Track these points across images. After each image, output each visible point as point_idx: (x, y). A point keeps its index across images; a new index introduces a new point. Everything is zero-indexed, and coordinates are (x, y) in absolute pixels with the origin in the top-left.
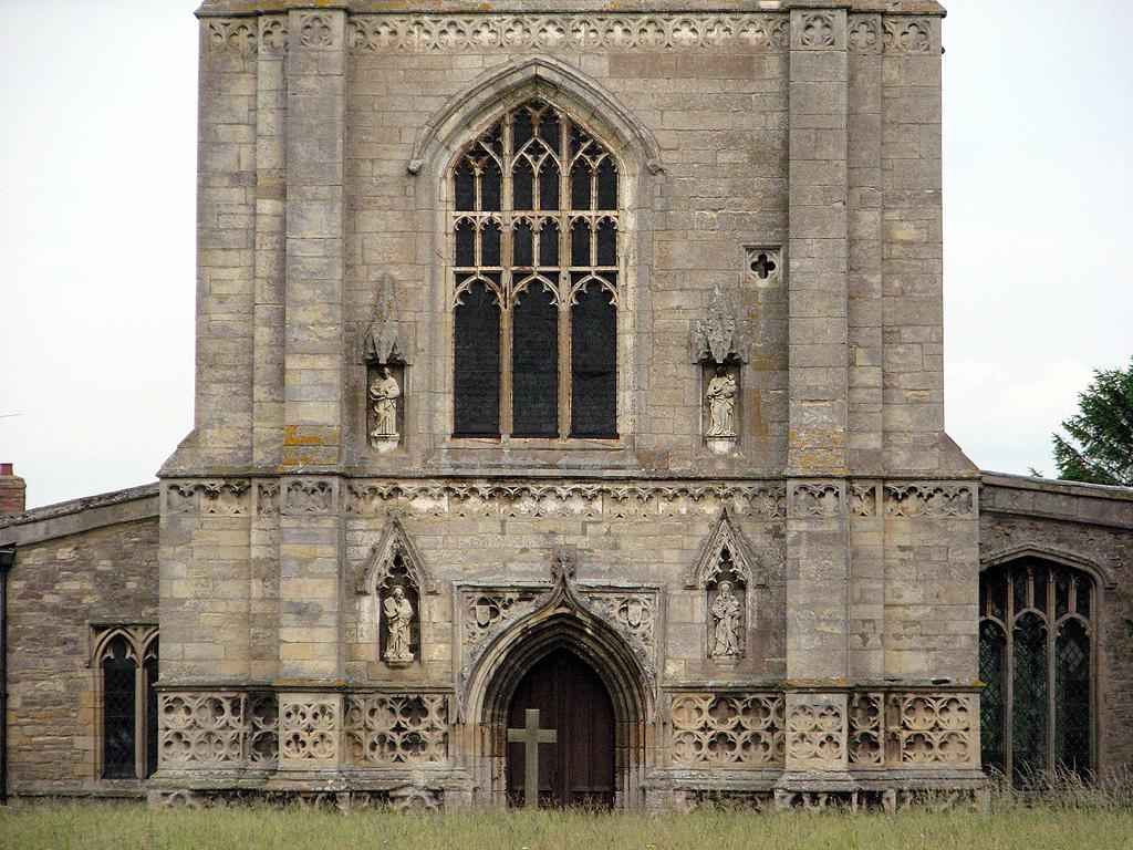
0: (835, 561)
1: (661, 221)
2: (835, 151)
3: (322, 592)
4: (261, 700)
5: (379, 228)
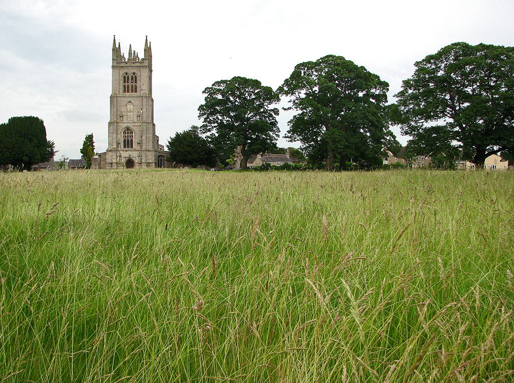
0: (145, 155)
1: (135, 135)
2: (145, 131)
3: (115, 157)
4: (111, 164)
5: (119, 136)
